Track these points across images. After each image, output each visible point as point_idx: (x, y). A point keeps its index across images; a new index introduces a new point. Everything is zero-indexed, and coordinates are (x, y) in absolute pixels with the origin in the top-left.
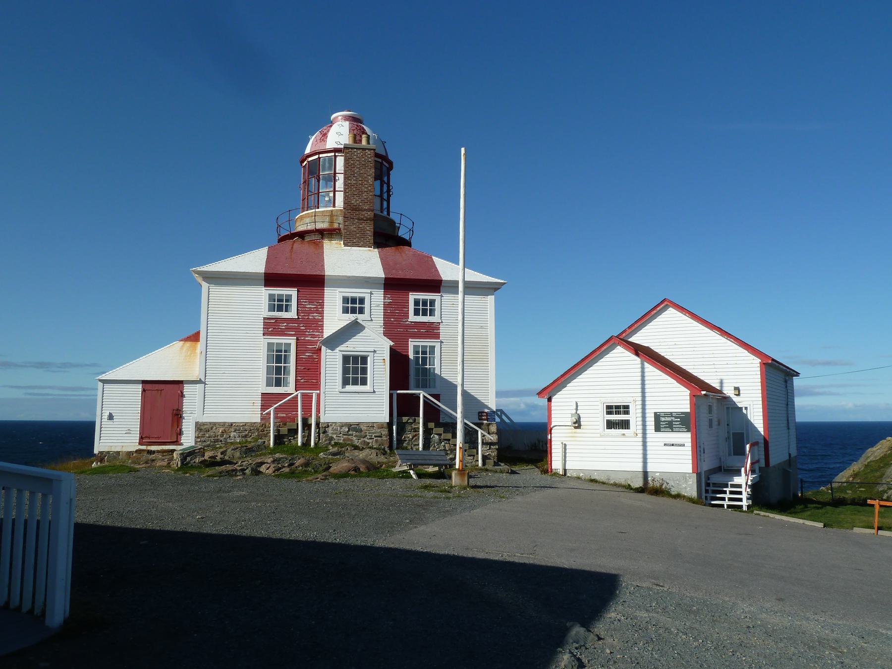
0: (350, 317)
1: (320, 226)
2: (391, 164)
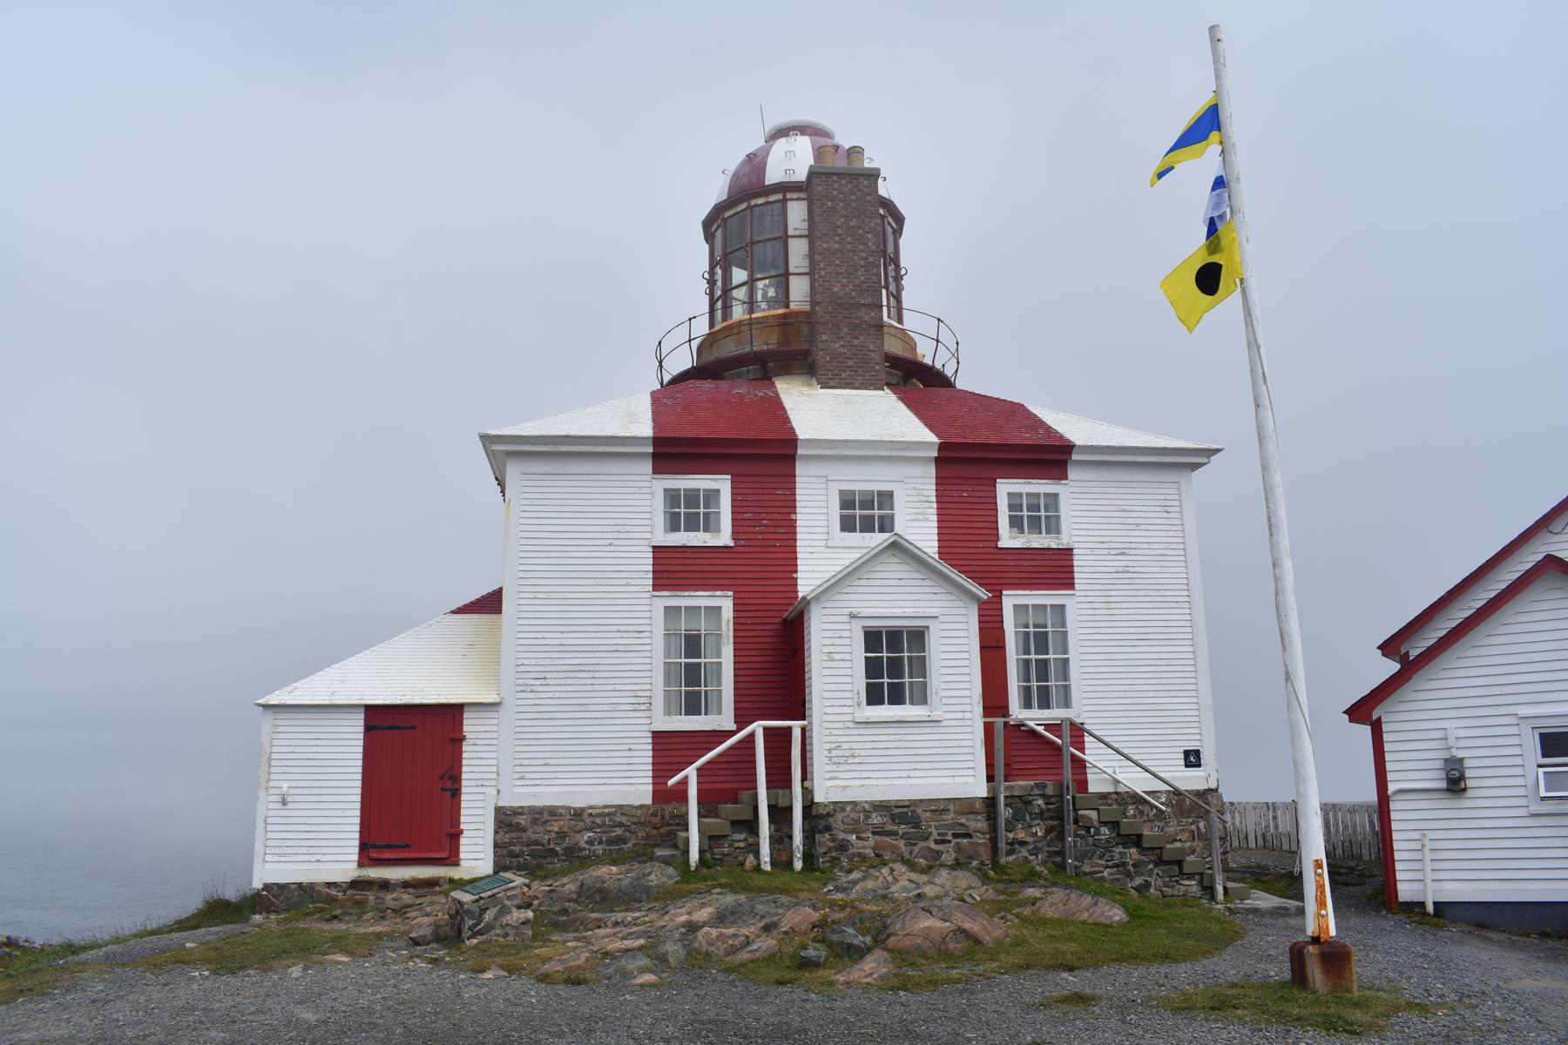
1: (758, 346)
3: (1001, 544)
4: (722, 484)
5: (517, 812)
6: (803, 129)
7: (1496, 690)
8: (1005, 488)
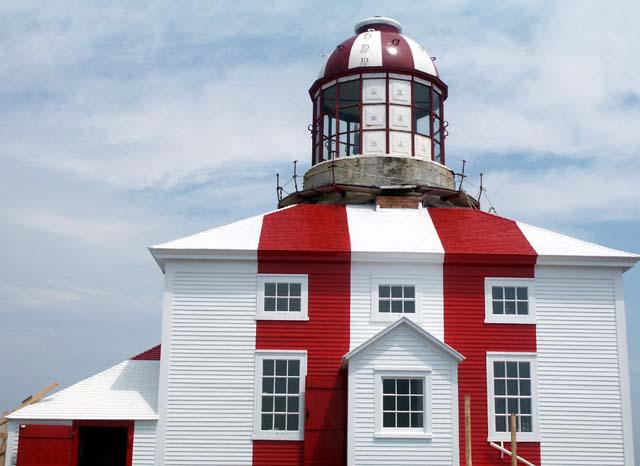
0: (394, 317)
2: (444, 88)
3: (486, 321)
6: (377, 26)
7: (441, 416)
8: (490, 283)
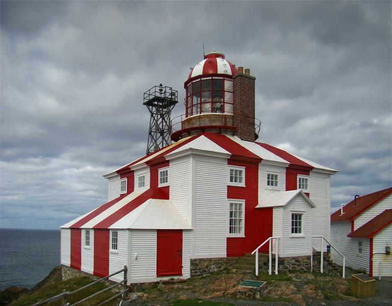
4: (243, 169)
5: (195, 260)
